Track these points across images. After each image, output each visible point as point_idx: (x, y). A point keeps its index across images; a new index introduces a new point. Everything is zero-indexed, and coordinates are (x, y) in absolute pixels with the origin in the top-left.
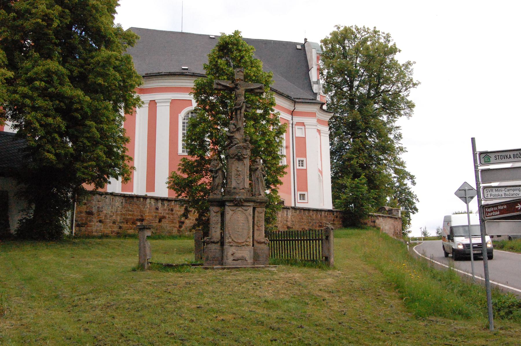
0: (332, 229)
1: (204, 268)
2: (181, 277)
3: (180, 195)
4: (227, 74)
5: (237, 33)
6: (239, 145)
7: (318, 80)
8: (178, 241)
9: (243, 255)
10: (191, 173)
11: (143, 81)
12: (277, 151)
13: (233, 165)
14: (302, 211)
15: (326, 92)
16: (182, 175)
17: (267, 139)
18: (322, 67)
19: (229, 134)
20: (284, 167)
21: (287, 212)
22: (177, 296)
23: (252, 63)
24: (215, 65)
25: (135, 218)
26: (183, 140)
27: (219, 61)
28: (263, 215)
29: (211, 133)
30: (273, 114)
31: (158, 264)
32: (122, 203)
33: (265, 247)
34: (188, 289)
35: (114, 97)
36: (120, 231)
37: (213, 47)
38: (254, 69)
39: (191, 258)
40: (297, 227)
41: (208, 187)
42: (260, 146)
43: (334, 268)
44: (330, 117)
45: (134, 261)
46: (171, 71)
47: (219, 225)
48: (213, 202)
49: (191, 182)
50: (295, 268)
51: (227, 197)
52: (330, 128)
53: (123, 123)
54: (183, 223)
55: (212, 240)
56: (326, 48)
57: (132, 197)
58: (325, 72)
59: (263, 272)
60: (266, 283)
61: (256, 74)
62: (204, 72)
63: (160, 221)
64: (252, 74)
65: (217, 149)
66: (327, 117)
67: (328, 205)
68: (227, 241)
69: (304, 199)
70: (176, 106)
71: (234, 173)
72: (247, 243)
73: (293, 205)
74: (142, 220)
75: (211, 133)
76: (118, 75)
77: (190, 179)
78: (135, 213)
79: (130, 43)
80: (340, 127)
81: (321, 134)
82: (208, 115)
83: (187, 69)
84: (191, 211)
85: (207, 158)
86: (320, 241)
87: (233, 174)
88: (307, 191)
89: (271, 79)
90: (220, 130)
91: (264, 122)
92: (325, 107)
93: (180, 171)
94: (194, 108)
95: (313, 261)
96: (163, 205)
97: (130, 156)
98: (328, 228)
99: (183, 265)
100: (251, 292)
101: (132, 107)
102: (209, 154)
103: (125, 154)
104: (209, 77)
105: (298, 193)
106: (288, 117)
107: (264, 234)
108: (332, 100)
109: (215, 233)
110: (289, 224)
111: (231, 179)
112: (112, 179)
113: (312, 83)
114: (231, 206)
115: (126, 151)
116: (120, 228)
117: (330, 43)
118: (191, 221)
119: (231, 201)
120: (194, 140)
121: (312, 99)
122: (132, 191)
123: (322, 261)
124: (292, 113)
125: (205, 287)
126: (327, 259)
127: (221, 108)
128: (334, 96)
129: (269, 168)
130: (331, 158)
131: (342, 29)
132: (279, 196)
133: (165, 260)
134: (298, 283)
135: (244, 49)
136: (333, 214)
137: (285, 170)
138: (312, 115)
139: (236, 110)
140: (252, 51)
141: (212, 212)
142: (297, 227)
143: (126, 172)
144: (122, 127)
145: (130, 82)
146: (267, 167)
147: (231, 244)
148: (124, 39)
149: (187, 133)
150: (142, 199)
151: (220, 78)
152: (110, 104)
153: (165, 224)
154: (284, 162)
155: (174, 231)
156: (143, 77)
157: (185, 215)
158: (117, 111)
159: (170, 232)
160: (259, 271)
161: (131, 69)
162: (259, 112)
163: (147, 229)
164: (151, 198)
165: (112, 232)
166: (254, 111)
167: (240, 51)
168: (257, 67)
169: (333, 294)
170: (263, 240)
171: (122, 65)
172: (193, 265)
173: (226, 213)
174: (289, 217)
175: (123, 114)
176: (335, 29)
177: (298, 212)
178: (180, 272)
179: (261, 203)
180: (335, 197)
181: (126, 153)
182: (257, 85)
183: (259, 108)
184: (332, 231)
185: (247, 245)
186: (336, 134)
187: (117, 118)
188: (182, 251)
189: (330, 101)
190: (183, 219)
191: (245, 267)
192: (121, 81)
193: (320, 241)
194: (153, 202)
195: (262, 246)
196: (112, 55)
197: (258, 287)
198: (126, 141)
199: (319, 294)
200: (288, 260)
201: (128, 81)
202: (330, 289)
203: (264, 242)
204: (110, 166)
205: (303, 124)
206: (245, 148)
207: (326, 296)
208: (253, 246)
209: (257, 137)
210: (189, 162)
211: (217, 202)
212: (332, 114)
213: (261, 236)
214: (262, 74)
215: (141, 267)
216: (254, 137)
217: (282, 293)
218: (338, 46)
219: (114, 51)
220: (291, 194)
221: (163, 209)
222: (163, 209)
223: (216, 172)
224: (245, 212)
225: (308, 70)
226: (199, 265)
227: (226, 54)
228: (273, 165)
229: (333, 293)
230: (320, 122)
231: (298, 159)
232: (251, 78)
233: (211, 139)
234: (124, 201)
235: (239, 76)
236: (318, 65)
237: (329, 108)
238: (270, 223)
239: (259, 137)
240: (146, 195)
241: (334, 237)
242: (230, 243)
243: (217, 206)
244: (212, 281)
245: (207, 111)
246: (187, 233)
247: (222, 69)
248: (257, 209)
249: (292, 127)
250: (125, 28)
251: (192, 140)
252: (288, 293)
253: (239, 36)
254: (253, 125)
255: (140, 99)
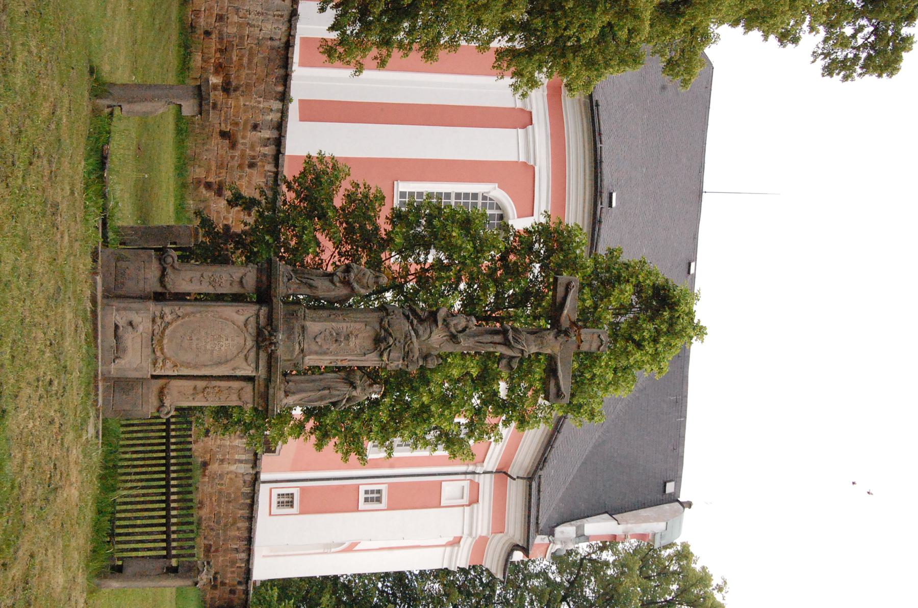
0: (196, 584)
1: (96, 248)
2: (72, 193)
3: (290, 188)
4: (596, 307)
5: (700, 331)
6: (414, 339)
7: (587, 539)
8: (172, 182)
9: (130, 350)
10: (345, 216)
11: (580, 95)
12: (402, 436)
13: (363, 325)
14: (248, 501)
15: (555, 557)
16: (342, 192)
17: (433, 408)
18: (620, 547)
19: (442, 313)
20: (361, 453)
21: (246, 462)
22: (20, 181)
23: (625, 369)
24: (618, 279)
25: (233, 72)
26: (430, 195)
27: (629, 288)
28: (233, 401)
29: (447, 268)
30: (496, 425)
31: (109, 132)
32: (271, 39)
33: (149, 408)
34: (38, 209)
35: (538, 23)
36: (200, 31)
37: (663, 270)
38: (610, 376)
39: (125, 216)
40: (204, 488)
41: (308, 259)
42: (414, 390)
43: (91, 592)
44: (493, 571)
45: (118, 69)
46: (604, 165)
47: (206, 288)
48: (267, 274)
49: (323, 216)
50: (93, 489)
51: (280, 309)
52: (462, 570)
53: (474, 44)
54: (219, 193)
55: (169, 270)
56: (670, 558)
57: (286, 63)
58: (608, 556)
59: (84, 403)
60: (52, 413)
61: (597, 380)
62: (602, 250)
63: (224, 135)
64: (597, 371)
65: (406, 282)
66: (493, 563)
67: (267, 567)
68: (167, 310)
69: (281, 504)
70: (519, 176)
71: (343, 326)
72: (160, 361)
73: (263, 477)
74: (227, 88)
75: (447, 268)
76: (594, 34)
77: (330, 214)
78: (244, 73)
79: (671, 64)
80: (469, 595)
81: (448, 549)
82: (492, 259)
83: (610, 205)
84: (249, 215)
85: (383, 256)
86: (164, 553)
87: (340, 325)
88: (302, 512)
89: (585, 419)
90: (456, 289)
91: (476, 401)
92: (518, 556)
93: (350, 187)
94: (510, 223)
95: (112, 535)
96: (266, 142)
97: (390, 60)
98: (199, 572)
99: (104, 196)
100: (30, 375)
101: (513, 69)
102: (393, 261)
103: (395, 50)
104: (589, 262)
105: (294, 489)
106: (492, 460)
107: (185, 404)
108: (537, 576)
109: (188, 279)
110: (214, 467)
111: (327, 319)
112: (331, 15)
113: (578, 522)
114: (258, 323)
115: (401, 53)
116: (207, 33)
117: (680, 566)
118: (224, 213)
119: (270, 318)
120: (429, 223)
121: (537, 523)
122: (302, 64)
123: (111, 557)
124: (502, 472)
125: (45, 255)
126: (118, 570)
127: (511, 292)
128: (547, 579)
129: (357, 416)
130: (387, 575)
131: (718, 597)
132: (285, 442)
133: (120, 148)
134: (51, 497)
135: (660, 348)
136: (240, 583)
137: (353, 457)
138: (499, 525)
139: (504, 332)
140: (656, 370)
141: (242, 270)
142: (208, 489)
143: (349, 52)
144: (463, 43)
145: (576, 63)
146: (362, 410)
147: (158, 320)
148: (683, 51)
149: (448, 206)
150: (280, 89)
151: (586, 290)
152: (518, 14)
153: (217, 146)
154: (374, 452)
155: (198, 170)
156: (591, 96)
157: (237, 200)
158: (504, 30)
159: (194, 159)
160: (88, 394)
161: (607, 65)
162: (502, 388)
163: (201, 105)
164: (284, 113)
165: (197, 13)
166: (504, 374)
167: (655, 341)
168: (615, 383)
169: (19, 590)
170: (167, 402)
171: (617, 46)
172: (104, 224)
173: (240, 307)
174: (233, 468)
175: (495, 44)
176: (716, 581)
177: (247, 490)
178: (87, 187)
179: (265, 397)
180: (285, 586)
181: (396, 53)
182: (565, 384)
183: (511, 390)
184: (189, 582)
185: (154, 364)
186: (449, 587)
187: (485, 31)
188: (144, 195)
189: (534, 568)
190: (228, 194)
191: (96, 357)
192: (579, 40)
193: (164, 553)
194: (275, 117)
195: (154, 401)
196: (643, 21)
197: (41, 391)
198: (428, 53)
199: (20, 553)
200: (115, 467)
201: (579, 59)
202: (34, 581)
203: (162, 405)
204: (364, 12)
205: (474, 500)
206: (406, 356)
207: (16, 571)
208: (154, 377)
209: (440, 385)
210: (374, 209)
211: (269, 286)
212: (500, 576)
213: (180, 396)
214: (596, 396)
215: (101, 89)
216: (437, 377)
217: (24, 455)
218: (674, 587)
219: (651, 26)
220: (293, 470)
221: (253, 141)
222: (253, 141)
223: (346, 283)
224: (242, 356)
225: (613, 511)
226: (105, 236)
227: (646, 305)
228: (367, 424)
229: (24, 589)
230: (481, 544)
231: (384, 488)
232: (586, 367)
233: (432, 266)
234: (276, 43)
235: (590, 339)
236: (626, 537)
237: (516, 568)
238: (216, 419)
239: (438, 390)
240: (291, 100)
241: (179, 589)
242: (162, 318)
243: (259, 281)
244: (62, 273)
245: (504, 258)
246: (191, 204)
247: (608, 295)
248: (248, 387)
249: (466, 473)
250: (710, 51)
251: (430, 218)
252: (26, 472)
253: (691, 338)
254: (468, 373)
255: (531, 88)
